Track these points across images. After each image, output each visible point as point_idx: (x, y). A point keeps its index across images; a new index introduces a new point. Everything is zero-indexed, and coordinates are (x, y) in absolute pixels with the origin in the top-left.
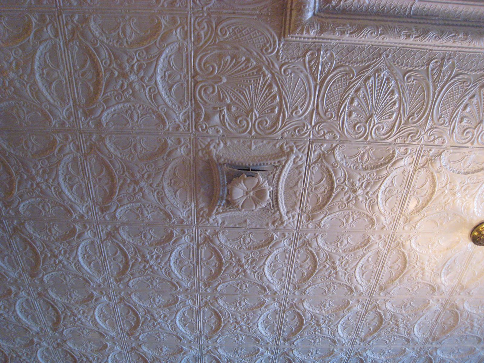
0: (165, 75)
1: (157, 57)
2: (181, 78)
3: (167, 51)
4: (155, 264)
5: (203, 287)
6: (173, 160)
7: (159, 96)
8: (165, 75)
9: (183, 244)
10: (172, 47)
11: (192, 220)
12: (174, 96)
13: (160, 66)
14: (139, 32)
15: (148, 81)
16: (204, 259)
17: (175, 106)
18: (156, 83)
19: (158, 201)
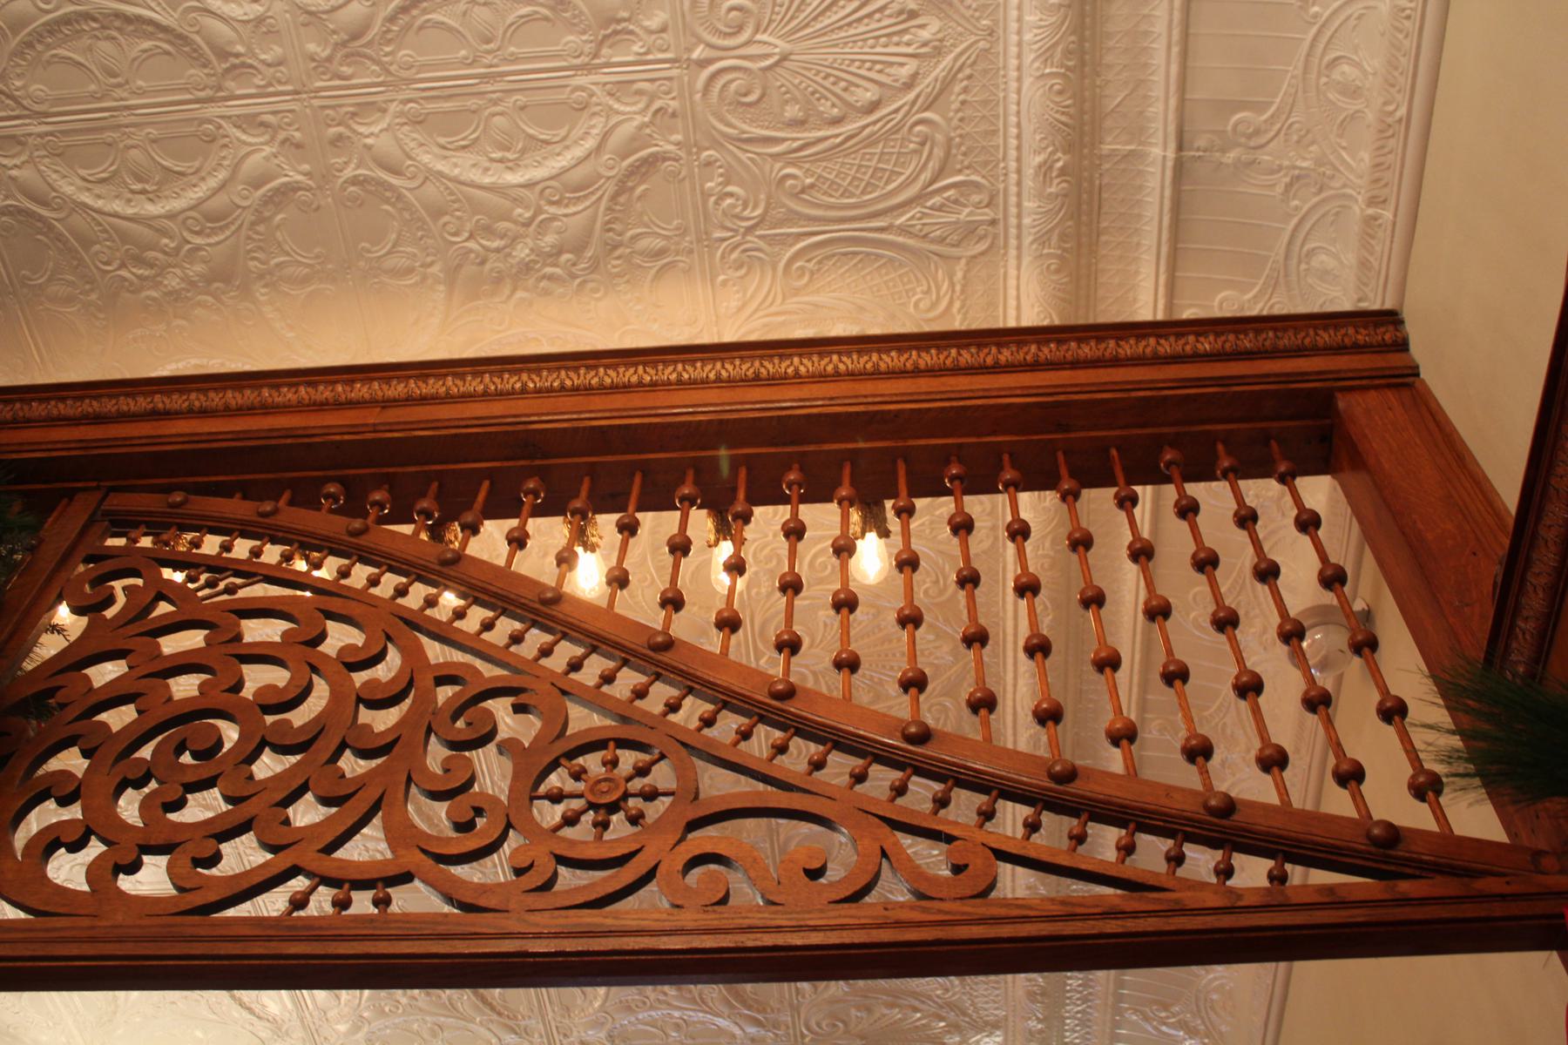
0: (501, 161)
1: (449, 184)
2: (501, 114)
3: (426, 158)
4: (178, 271)
5: (636, 48)
6: (411, 158)
7: (205, 206)
8: (501, 161)
9: (398, 140)
10: (412, 145)
11: (274, 113)
12: (197, 164)
13: (117, 206)
14: (394, 236)
15: (527, 208)
16: (463, 53)
17: (224, 158)
18: (529, 185)
19: (228, 233)
